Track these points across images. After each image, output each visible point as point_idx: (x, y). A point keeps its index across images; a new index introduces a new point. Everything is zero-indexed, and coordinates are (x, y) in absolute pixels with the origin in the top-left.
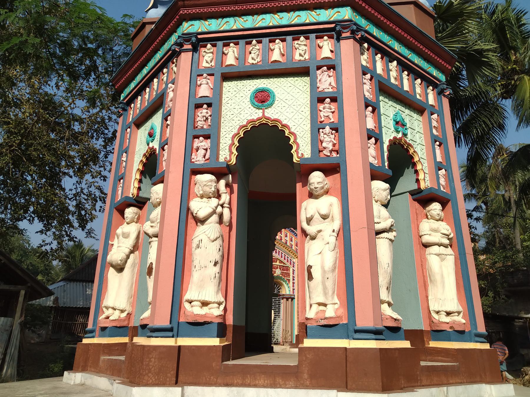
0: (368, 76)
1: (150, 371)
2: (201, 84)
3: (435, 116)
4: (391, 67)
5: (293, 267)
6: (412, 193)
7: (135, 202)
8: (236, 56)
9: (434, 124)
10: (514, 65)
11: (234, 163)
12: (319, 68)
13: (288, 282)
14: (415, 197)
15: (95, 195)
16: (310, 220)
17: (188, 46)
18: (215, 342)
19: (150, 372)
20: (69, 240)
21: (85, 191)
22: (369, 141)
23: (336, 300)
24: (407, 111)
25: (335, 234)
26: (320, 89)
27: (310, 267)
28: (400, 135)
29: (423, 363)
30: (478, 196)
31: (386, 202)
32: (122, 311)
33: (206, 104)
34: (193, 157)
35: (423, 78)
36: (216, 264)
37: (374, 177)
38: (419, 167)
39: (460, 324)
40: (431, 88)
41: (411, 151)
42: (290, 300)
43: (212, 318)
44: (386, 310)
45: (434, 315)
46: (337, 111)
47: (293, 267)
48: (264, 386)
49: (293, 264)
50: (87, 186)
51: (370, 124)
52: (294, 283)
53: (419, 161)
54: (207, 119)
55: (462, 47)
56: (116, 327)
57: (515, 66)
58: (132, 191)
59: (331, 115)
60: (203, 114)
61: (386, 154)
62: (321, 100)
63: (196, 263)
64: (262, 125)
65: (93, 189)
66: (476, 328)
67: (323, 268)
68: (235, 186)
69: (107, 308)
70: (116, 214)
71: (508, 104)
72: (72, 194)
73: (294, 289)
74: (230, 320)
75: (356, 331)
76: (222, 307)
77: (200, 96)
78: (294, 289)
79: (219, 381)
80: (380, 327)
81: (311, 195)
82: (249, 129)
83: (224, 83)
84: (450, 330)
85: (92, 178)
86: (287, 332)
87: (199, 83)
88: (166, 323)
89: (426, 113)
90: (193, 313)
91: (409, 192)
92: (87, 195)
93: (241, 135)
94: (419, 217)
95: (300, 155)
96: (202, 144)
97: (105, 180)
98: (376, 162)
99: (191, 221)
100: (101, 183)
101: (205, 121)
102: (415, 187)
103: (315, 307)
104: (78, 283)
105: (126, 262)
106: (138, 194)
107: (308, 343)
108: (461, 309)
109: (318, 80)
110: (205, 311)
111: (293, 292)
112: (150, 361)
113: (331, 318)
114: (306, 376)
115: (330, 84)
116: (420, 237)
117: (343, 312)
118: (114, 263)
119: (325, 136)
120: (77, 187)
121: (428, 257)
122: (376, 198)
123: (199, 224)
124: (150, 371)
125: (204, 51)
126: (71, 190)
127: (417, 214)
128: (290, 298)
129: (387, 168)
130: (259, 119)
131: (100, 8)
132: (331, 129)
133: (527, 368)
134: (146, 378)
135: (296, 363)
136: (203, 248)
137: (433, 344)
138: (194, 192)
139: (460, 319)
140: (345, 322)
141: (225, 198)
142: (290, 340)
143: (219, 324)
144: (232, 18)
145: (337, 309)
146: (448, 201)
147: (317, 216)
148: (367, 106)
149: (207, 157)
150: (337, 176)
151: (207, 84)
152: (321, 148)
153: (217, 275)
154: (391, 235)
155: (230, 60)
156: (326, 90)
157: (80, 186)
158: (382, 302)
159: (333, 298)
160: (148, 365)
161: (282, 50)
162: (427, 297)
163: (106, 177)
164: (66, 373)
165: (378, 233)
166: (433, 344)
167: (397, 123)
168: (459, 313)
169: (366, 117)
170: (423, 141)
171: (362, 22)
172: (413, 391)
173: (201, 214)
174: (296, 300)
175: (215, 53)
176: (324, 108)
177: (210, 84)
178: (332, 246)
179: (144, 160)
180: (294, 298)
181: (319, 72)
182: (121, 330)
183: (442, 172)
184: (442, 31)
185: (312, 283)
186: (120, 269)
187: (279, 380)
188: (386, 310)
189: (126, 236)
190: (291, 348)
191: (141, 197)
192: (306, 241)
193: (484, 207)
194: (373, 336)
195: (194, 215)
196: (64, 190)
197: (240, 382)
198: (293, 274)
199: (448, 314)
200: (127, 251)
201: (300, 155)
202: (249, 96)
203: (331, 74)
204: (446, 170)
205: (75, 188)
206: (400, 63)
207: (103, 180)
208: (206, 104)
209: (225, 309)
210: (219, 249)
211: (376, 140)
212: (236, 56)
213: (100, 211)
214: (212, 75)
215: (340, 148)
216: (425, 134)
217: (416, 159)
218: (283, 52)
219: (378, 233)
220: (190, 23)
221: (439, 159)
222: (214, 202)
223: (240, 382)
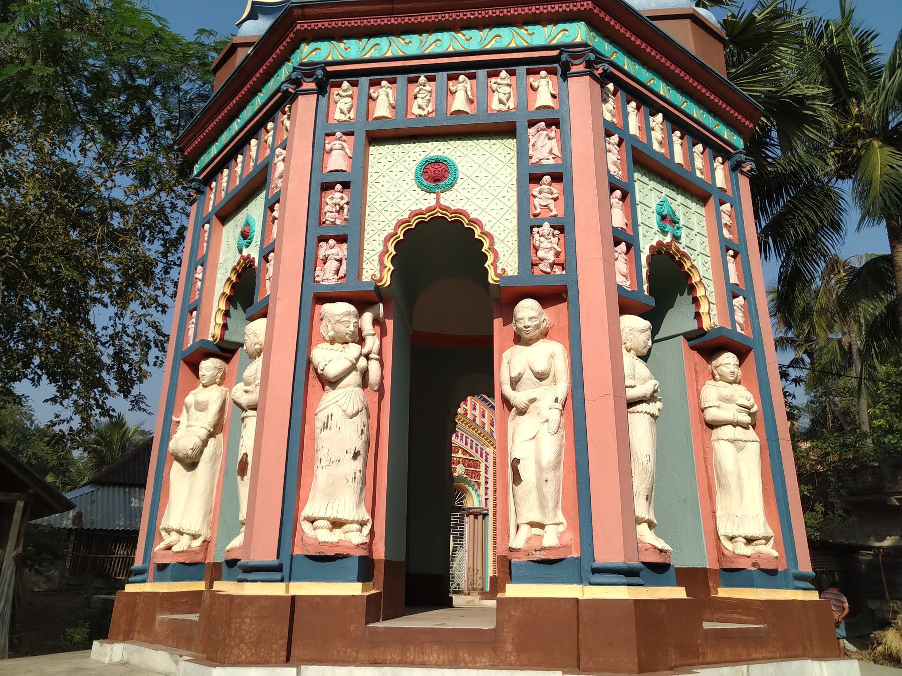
0: (615, 139)
1: (242, 640)
2: (331, 150)
3: (727, 207)
4: (652, 124)
5: (486, 461)
6: (689, 337)
7: (217, 350)
8: (392, 102)
9: (726, 219)
11: (388, 283)
12: (532, 124)
13: (476, 487)
14: (693, 342)
15: (147, 337)
16: (517, 382)
17: (309, 85)
18: (354, 589)
21: (130, 331)
22: (617, 249)
23: (561, 518)
24: (680, 199)
26: (534, 160)
27: (516, 461)
28: (668, 239)
29: (707, 625)
31: (645, 351)
32: (194, 537)
33: (340, 183)
34: (317, 273)
36: (356, 456)
38: (700, 293)
39: (768, 558)
40: (720, 159)
41: (687, 266)
42: (480, 517)
43: (349, 548)
44: (646, 535)
46: (562, 198)
47: (486, 461)
49: (486, 457)
50: (133, 321)
51: (619, 219)
52: (486, 489)
53: (700, 282)
54: (342, 208)
56: (184, 564)
58: (213, 331)
59: (552, 204)
60: (334, 201)
61: (644, 271)
62: (536, 179)
63: (322, 454)
64: (438, 221)
65: (143, 327)
66: (796, 565)
67: (538, 463)
69: (168, 531)
72: (106, 336)
73: (487, 499)
74: (380, 552)
75: (595, 571)
76: (366, 529)
78: (487, 499)
79: (361, 656)
80: (635, 563)
82: (413, 226)
83: (371, 148)
84: (753, 569)
85: (142, 309)
86: (475, 572)
87: (328, 147)
88: (268, 557)
89: (712, 202)
90: (316, 539)
92: (133, 338)
93: (399, 237)
94: (701, 377)
95: (499, 271)
96: (333, 250)
97: (164, 312)
99: (314, 383)
100: (157, 317)
101: (338, 212)
102: (693, 326)
103: (525, 529)
104: (116, 489)
105: (201, 452)
106: (222, 335)
107: (513, 591)
108: (770, 532)
109: (531, 144)
110: (336, 536)
111: (486, 504)
112: (243, 622)
113: (552, 548)
114: (509, 647)
115: (551, 152)
116: (703, 410)
117: (572, 538)
118: (180, 454)
119: (543, 239)
120: (115, 323)
121: (716, 444)
122: (629, 345)
123: (327, 387)
126: (105, 328)
127: (696, 372)
128: (480, 514)
129: (646, 293)
130: (430, 209)
131: (158, 18)
132: (551, 227)
133: (880, 632)
134: (236, 651)
135: (492, 626)
136: (334, 428)
137: (724, 592)
138: (320, 334)
139: (769, 550)
140: (576, 555)
141: (372, 343)
142: (481, 587)
143: (361, 558)
145: (562, 534)
146: (749, 350)
147: (528, 375)
148: (612, 189)
149: (341, 273)
151: (343, 149)
152: (534, 259)
153: (358, 475)
155: (382, 109)
156: (544, 162)
158: (639, 521)
159: (555, 514)
160: (239, 629)
161: (469, 93)
162: (714, 512)
163: (166, 306)
164: (96, 644)
165: (632, 403)
166: (724, 592)
167: (663, 218)
168: (767, 539)
169: (611, 207)
170: (707, 249)
171: (605, 48)
173: (332, 371)
174: (490, 518)
175: (355, 97)
176: (540, 193)
177: (347, 150)
178: (553, 425)
179: (234, 278)
181: (532, 131)
182: (192, 568)
183: (739, 301)
185: (520, 489)
186: (191, 464)
187: (465, 655)
188: (646, 535)
189: (202, 407)
190: (482, 599)
191: (228, 342)
192: (510, 418)
193: (807, 360)
194: (624, 579)
195: (320, 372)
196: (93, 328)
197: (397, 658)
198: (486, 473)
199: (750, 541)
200: (203, 433)
201: (499, 271)
202: (413, 171)
203: (553, 134)
204: (745, 299)
205: (112, 326)
206: (668, 117)
207: (162, 311)
208: (340, 183)
209: (372, 534)
210: (362, 430)
211: (629, 247)
212: (392, 102)
213: (155, 365)
214: (351, 134)
216: (710, 236)
217: (695, 279)
219: (632, 403)
220: (313, 45)
221: (733, 279)
222: (354, 349)
223: (397, 658)
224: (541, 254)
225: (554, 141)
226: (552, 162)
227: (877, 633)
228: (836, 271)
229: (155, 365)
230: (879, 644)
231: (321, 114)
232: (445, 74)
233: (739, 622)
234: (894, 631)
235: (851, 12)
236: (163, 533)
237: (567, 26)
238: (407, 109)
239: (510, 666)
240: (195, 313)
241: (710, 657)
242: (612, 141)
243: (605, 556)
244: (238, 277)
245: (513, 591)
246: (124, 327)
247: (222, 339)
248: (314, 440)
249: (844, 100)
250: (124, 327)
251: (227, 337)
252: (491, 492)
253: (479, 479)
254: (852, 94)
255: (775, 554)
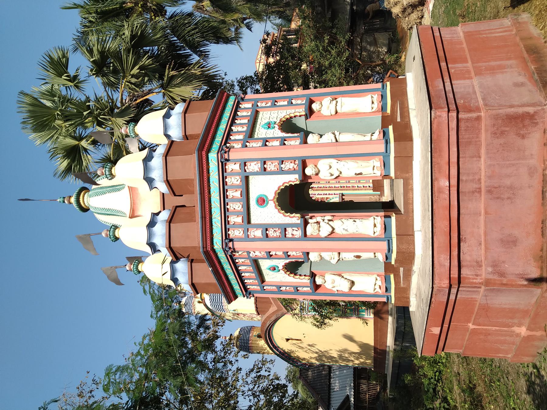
0: (247, 144)
1: (408, 248)
2: (254, 235)
3: (259, 104)
4: (236, 131)
5: (315, 195)
6: (307, 119)
8: (236, 216)
9: (264, 105)
10: (138, 6)
11: (299, 215)
12: (245, 171)
16: (331, 174)
18: (393, 218)
19: (409, 248)
20: (296, 398)
21: (251, 387)
22: (287, 144)
24: (259, 121)
25: (339, 162)
26: (258, 170)
27: (356, 174)
28: (276, 126)
29: (399, 120)
30: (237, 26)
31: (319, 136)
32: (377, 279)
34: (297, 237)
35: (236, 111)
37: (305, 142)
38: (292, 115)
39: (378, 98)
41: (284, 119)
42: (344, 197)
43: (382, 221)
45: (373, 110)
47: (315, 195)
48: (413, 194)
49: (313, 195)
50: (246, 386)
51: (277, 143)
52: (329, 194)
53: (289, 115)
54: (275, 231)
55: (132, 54)
57: (139, 5)
58: (306, 280)
59: (274, 164)
61: (290, 135)
62: (265, 169)
64: (278, 201)
65: (249, 380)
68: (311, 215)
69: (375, 289)
70: (319, 291)
71: (170, 10)
72: (254, 400)
73: (334, 194)
74: (382, 214)
75: (386, 152)
76: (376, 217)
77: (261, 236)
78: (334, 194)
80: (384, 141)
81: (317, 174)
84: (381, 103)
85: (239, 382)
87: (253, 237)
88: (385, 244)
89: (258, 109)
91: (306, 120)
95: (296, 180)
96: (289, 231)
97: (240, 369)
98: (298, 141)
99: (332, 236)
100: (243, 372)
102: (303, 117)
106: (308, 276)
107: (392, 174)
109: (253, 171)
111: (337, 194)
112: (404, 248)
114: (407, 175)
115: (256, 165)
117: (377, 158)
120: (248, 395)
123: (334, 231)
124: (408, 248)
125: (232, 236)
126: (250, 400)
128: (342, 197)
129: (299, 134)
130: (275, 203)
131: (144, 337)
133: (393, 15)
134: (411, 249)
137: (389, 111)
140: (382, 157)
142: (378, 196)
143: (384, 218)
144: (213, 220)
146: (310, 99)
148: (266, 145)
149: (297, 229)
150: (307, 161)
152: (293, 169)
153: (361, 220)
154: (337, 133)
155: (239, 220)
156: (260, 166)
157: (247, 392)
158: (371, 139)
163: (237, 368)
166: (389, 111)
168: (372, 97)
169: (272, 146)
170: (276, 111)
172: (347, 334)
173: (331, 230)
174: (344, 192)
175: (234, 229)
176: (270, 168)
179: (288, 273)
180: (342, 193)
181: (247, 171)
183: (294, 102)
184: (480, 190)
186: (353, 283)
187: (406, 109)
189: (334, 282)
190: (384, 196)
192: (342, 176)
193: (247, 21)
194: (388, 144)
195: (330, 233)
197: (411, 205)
198: (321, 195)
201: (296, 180)
204: (292, 99)
205: (249, 397)
206: (231, 125)
207: (240, 370)
209: (377, 216)
211: (285, 140)
212: (236, 216)
213: (270, 372)
214: (248, 229)
215: (293, 159)
217: (288, 117)
218: (235, 191)
219: (337, 141)
220: (215, 244)
221: (286, 103)
222: (322, 224)
224: (291, 167)
225: (251, 164)
226: (259, 164)
227: (393, 16)
228: (202, 7)
229: (270, 372)
230: (398, 15)
231: (240, 240)
232: (226, 199)
233: (397, 108)
234: (392, 9)
235: (75, 4)
236: (375, 292)
237: (210, 159)
238: (239, 212)
239: (412, 174)
240: (298, 289)
241: (408, 120)
242: (249, 145)
243: (382, 148)
244: (288, 271)
245: (392, 174)
246: (249, 390)
247: (309, 276)
248: (350, 234)
249: (124, 10)
250: (249, 390)
251: (309, 275)
252: (331, 192)
253: (325, 198)
254: (121, 7)
255: (376, 95)
